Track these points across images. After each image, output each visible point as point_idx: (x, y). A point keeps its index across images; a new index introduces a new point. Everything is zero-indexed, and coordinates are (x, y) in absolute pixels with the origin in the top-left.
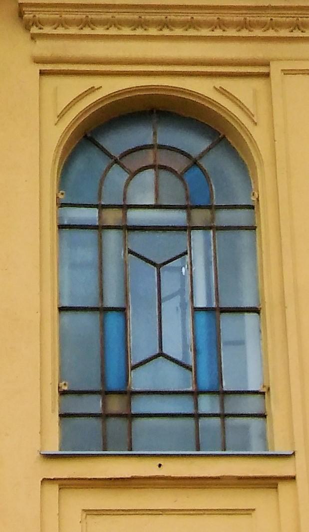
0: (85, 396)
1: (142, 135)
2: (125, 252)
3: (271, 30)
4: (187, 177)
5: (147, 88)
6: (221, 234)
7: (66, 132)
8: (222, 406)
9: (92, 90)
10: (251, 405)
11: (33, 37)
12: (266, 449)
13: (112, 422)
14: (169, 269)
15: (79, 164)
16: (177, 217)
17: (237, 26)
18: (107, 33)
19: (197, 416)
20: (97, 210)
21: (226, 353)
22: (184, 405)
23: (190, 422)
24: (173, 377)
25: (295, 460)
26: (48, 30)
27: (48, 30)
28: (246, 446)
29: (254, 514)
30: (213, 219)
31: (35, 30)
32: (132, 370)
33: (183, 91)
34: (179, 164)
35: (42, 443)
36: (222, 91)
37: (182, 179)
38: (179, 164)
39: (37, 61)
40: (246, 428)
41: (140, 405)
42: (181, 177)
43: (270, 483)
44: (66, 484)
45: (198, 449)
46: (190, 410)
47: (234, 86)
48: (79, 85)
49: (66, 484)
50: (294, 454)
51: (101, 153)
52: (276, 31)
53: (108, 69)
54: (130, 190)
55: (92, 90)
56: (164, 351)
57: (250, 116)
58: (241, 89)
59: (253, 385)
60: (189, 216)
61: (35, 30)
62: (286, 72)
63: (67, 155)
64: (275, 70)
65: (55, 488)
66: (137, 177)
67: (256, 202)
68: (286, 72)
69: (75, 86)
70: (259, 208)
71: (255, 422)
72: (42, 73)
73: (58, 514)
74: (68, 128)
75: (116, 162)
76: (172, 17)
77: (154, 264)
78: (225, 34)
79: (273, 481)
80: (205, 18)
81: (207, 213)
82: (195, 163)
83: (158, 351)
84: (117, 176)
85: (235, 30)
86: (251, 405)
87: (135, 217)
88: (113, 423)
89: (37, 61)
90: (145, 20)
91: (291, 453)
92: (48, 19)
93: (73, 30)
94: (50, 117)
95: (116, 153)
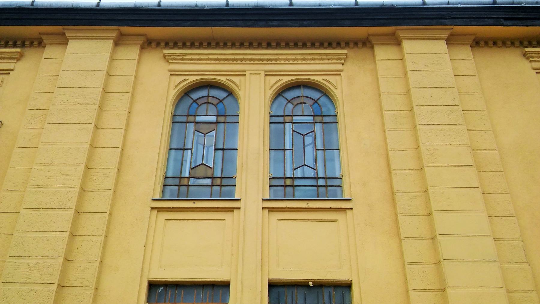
1: (204, 93)
2: (292, 131)
3: (339, 60)
4: (218, 106)
6: (325, 125)
7: (272, 93)
8: (326, 183)
9: (279, 80)
10: (336, 182)
11: (531, 62)
12: (342, 197)
13: (320, 188)
14: (309, 136)
15: (277, 102)
16: (310, 119)
17: (302, 60)
18: (285, 62)
19: (318, 186)
20: (312, 117)
21: (184, 162)
22: (313, 182)
23: (315, 188)
24: (310, 173)
25: (241, 202)
26: (535, 59)
27: (535, 59)
28: (336, 196)
30: (322, 120)
31: (531, 59)
32: (191, 169)
33: (309, 79)
34: (215, 101)
35: (263, 196)
36: (326, 80)
37: (216, 106)
38: (215, 101)
39: (169, 71)
40: (336, 191)
42: (215, 106)
43: (344, 210)
45: (318, 197)
46: (316, 184)
47: (233, 78)
48: (277, 78)
49: (271, 209)
50: (241, 199)
54: (294, 111)
55: (279, 80)
56: (306, 164)
57: (333, 86)
58: (236, 79)
59: (338, 175)
60: (225, 119)
61: (531, 59)
62: (251, 74)
63: (273, 100)
64: (247, 73)
65: (266, 211)
66: (201, 106)
67: (337, 113)
68: (251, 74)
69: (274, 79)
70: (338, 116)
71: (338, 188)
72: (171, 75)
73: (244, 221)
74: (273, 91)
75: (289, 102)
76: (533, 55)
77: (302, 135)
78: (298, 62)
80: (247, 58)
81: (320, 118)
82: (316, 102)
83: (201, 163)
84: (290, 106)
86: (336, 182)
87: (295, 119)
88: (321, 189)
89: (534, 69)
90: (184, 58)
91: (240, 199)
92: (535, 56)
94: (268, 87)
95: (289, 99)
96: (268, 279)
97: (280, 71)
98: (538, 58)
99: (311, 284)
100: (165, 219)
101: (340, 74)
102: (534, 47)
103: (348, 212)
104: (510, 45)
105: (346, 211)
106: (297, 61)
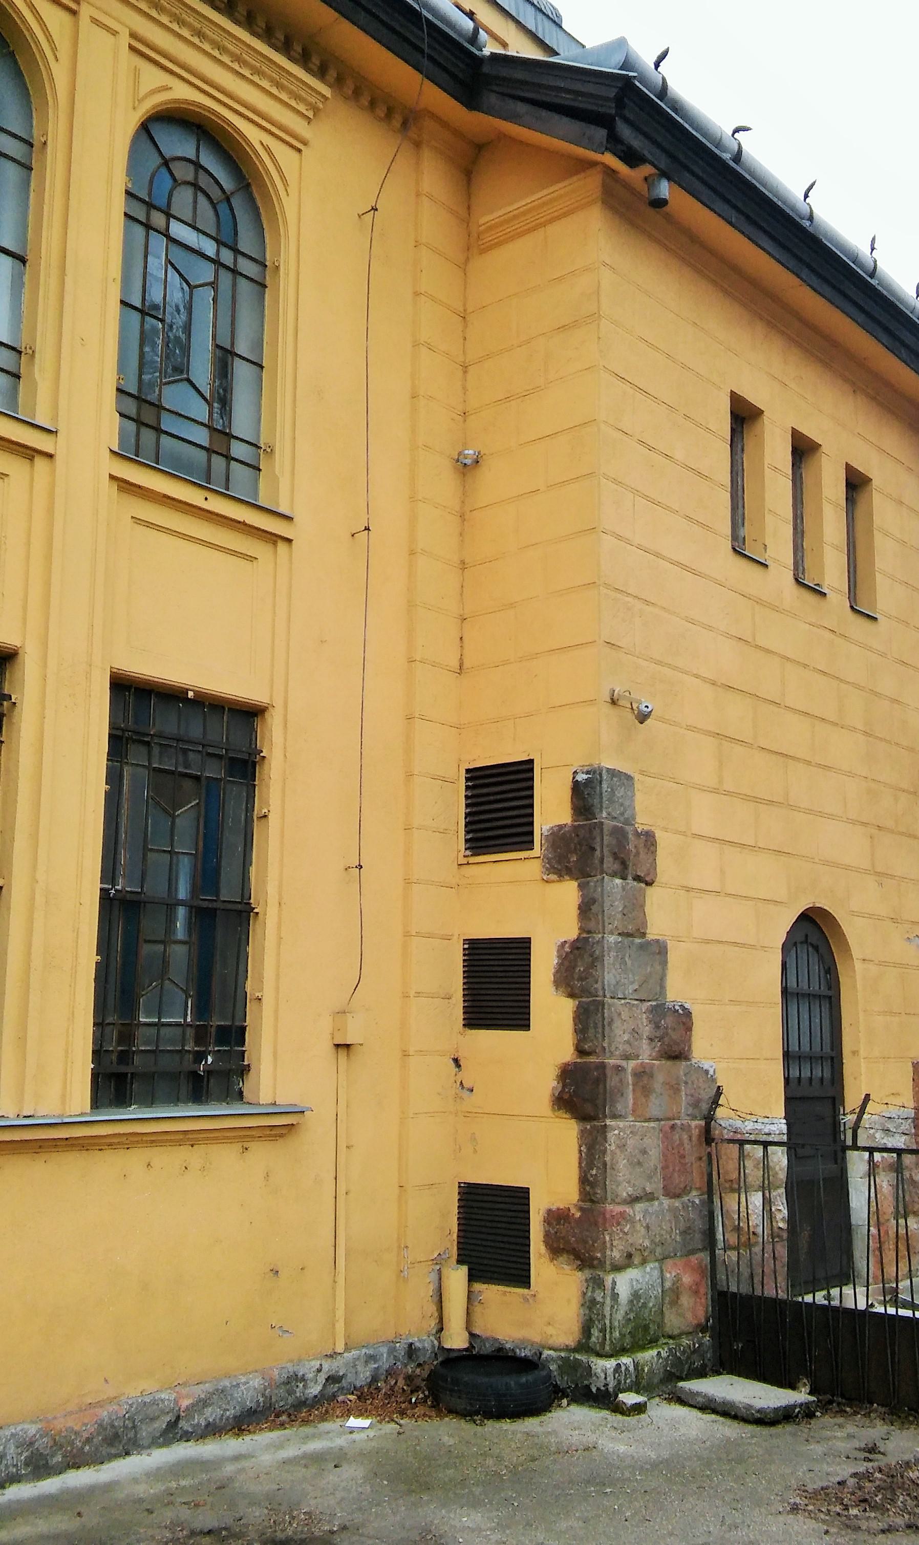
0: (182, 419)
5: (214, 112)
9: (167, 88)
29: (255, 562)
33: (230, 124)
36: (267, 149)
38: (216, 194)
41: (167, 422)
44: (125, 486)
48: (164, 79)
51: (152, 145)
52: (297, 103)
53: (144, 51)
55: (167, 88)
62: (95, 21)
69: (152, 77)
78: (200, 44)
79: (275, 538)
85: (169, 19)
93: (185, 33)
96: (111, 667)
97: (148, 45)
98: (309, 107)
99: (191, 694)
100: (132, 517)
101: (299, 151)
102: (290, 58)
103: (39, 462)
104: (223, 5)
105: (33, 457)
106: (201, 41)
